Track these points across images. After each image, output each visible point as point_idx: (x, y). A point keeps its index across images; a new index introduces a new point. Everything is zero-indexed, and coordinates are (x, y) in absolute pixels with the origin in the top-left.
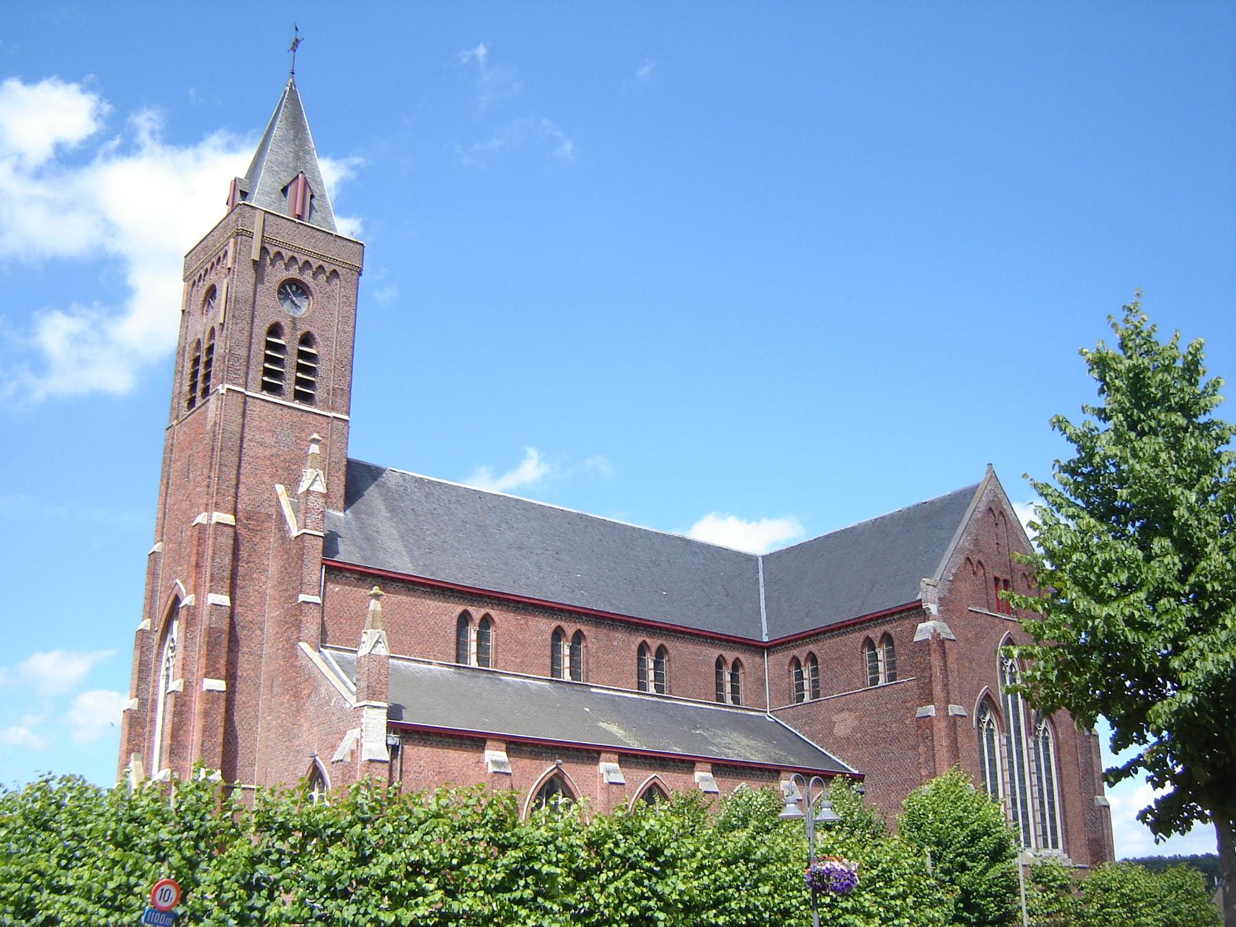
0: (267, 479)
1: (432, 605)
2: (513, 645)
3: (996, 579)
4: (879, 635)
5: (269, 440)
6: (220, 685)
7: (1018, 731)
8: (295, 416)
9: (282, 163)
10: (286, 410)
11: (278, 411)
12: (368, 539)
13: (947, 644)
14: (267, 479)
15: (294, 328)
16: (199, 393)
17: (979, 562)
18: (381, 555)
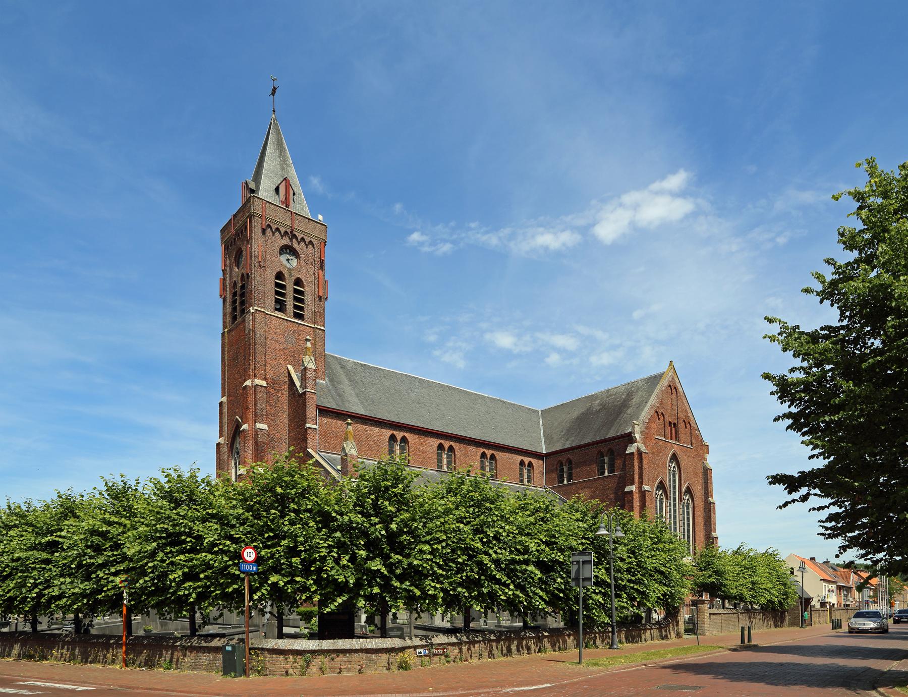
0: (282, 362)
1: (375, 430)
3: (670, 423)
7: (674, 500)
8: (295, 327)
9: (273, 171)
11: (286, 324)
12: (340, 396)
13: (644, 455)
14: (282, 362)
15: (290, 275)
16: (238, 313)
18: (347, 404)
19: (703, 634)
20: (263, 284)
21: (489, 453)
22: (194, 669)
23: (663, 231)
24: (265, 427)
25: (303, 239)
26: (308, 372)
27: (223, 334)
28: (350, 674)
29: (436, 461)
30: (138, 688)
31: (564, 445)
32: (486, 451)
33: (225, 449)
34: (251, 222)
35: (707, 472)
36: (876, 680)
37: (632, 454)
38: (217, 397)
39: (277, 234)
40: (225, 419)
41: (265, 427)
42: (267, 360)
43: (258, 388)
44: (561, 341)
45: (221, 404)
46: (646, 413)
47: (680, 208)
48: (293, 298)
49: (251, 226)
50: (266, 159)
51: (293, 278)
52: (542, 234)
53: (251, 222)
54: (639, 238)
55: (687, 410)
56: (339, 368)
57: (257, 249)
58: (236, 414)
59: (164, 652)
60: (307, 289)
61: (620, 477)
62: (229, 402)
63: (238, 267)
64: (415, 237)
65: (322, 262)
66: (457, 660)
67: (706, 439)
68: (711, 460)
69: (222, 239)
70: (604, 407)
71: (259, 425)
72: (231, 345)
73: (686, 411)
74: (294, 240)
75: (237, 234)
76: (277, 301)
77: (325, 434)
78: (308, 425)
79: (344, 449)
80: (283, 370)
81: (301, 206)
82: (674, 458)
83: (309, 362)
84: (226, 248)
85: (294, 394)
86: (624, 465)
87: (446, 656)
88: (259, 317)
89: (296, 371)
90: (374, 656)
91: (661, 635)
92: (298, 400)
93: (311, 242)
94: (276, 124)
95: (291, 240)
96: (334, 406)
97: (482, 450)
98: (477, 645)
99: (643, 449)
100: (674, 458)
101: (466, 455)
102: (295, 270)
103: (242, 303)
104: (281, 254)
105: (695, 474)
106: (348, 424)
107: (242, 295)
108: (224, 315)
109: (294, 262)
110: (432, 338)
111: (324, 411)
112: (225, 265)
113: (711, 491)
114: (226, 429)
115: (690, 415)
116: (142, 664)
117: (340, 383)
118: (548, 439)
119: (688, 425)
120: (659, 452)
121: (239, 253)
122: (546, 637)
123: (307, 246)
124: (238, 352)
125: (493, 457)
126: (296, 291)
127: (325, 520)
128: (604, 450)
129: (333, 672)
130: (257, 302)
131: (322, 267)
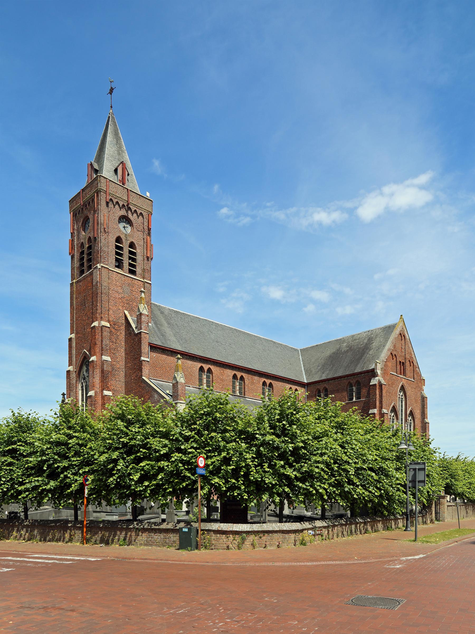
0: (120, 308)
2: (219, 380)
3: (400, 362)
4: (355, 381)
5: (121, 291)
6: (106, 393)
7: (402, 420)
8: (130, 281)
10: (126, 277)
12: (163, 335)
14: (120, 308)
15: (127, 240)
17: (395, 355)
19: (443, 521)
20: (107, 246)
21: (268, 381)
22: (145, 545)
23: (410, 213)
24: (109, 359)
25: (135, 211)
26: (143, 317)
27: (72, 285)
28: (272, 548)
29: (231, 387)
30: (134, 559)
31: (321, 376)
32: (266, 380)
33: (74, 375)
34: (97, 196)
35: (424, 399)
36: (32, 552)
37: (375, 385)
38: (66, 334)
39: (117, 206)
40: (74, 352)
41: (109, 359)
42: (110, 306)
43: (104, 328)
44: (318, 295)
45: (70, 340)
46: (384, 354)
47: (423, 197)
48: (129, 258)
49: (98, 200)
50: (107, 145)
51: (129, 242)
52: (319, 213)
53: (97, 196)
54: (389, 217)
55: (411, 353)
56: (159, 314)
57: (102, 218)
58: (84, 348)
59: (118, 533)
60: (139, 251)
61: (365, 402)
62: (77, 338)
63: (84, 230)
64: (225, 211)
65: (149, 230)
66: (327, 539)
67: (424, 376)
68: (427, 391)
69: (71, 208)
70: (350, 348)
71: (104, 358)
72: (79, 293)
73: (411, 354)
74: (129, 212)
75: (85, 205)
76: (117, 260)
77: (154, 366)
78: (142, 358)
79: (175, 378)
80: (121, 315)
81: (133, 184)
82: (403, 388)
83: (144, 310)
84: (75, 215)
85: (130, 333)
86: (369, 394)
87: (322, 536)
88: (104, 272)
89: (131, 316)
90: (287, 536)
91: (423, 522)
92: (134, 339)
93: (141, 214)
94: (113, 118)
95: (127, 212)
96: (160, 344)
97: (264, 379)
98: (336, 528)
99: (383, 382)
100: (403, 388)
101: (253, 383)
102: (129, 235)
103: (89, 260)
104: (119, 222)
105: (416, 401)
106: (178, 359)
107: (90, 254)
108: (73, 269)
109: (129, 229)
110: (222, 290)
111: (154, 348)
112: (73, 229)
113: (427, 414)
114: (74, 359)
115: (413, 356)
116: (98, 542)
117: (161, 325)
118: (308, 372)
119: (412, 364)
120: (393, 384)
121: (86, 220)
122: (369, 522)
123: (138, 217)
124: (85, 301)
125: (271, 385)
126: (130, 252)
127: (249, 438)
128: (353, 381)
129: (261, 547)
130: (102, 260)
131: (149, 234)
